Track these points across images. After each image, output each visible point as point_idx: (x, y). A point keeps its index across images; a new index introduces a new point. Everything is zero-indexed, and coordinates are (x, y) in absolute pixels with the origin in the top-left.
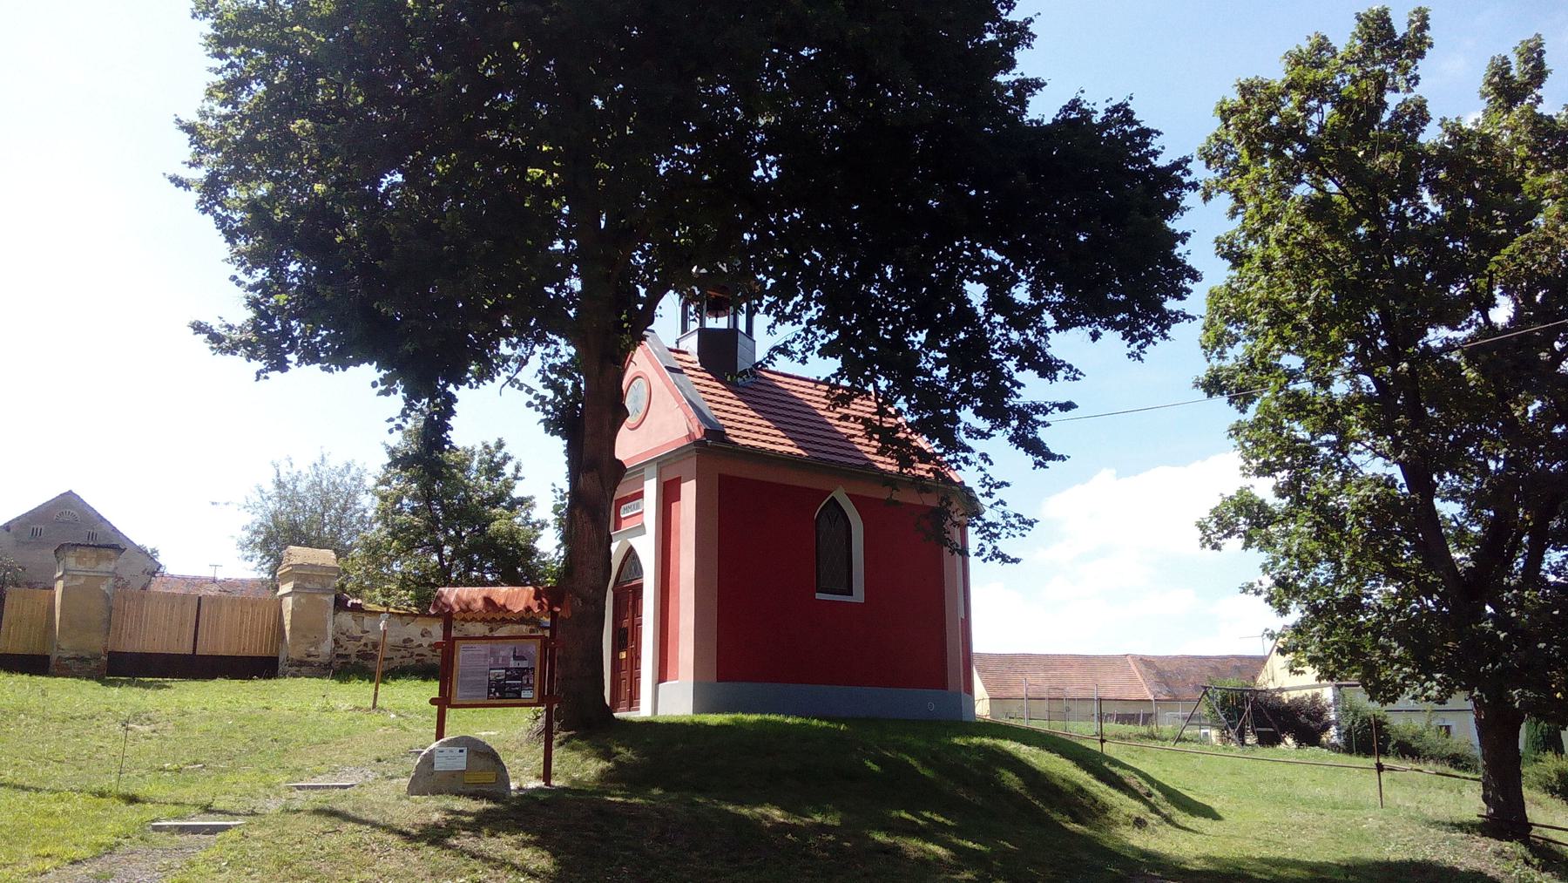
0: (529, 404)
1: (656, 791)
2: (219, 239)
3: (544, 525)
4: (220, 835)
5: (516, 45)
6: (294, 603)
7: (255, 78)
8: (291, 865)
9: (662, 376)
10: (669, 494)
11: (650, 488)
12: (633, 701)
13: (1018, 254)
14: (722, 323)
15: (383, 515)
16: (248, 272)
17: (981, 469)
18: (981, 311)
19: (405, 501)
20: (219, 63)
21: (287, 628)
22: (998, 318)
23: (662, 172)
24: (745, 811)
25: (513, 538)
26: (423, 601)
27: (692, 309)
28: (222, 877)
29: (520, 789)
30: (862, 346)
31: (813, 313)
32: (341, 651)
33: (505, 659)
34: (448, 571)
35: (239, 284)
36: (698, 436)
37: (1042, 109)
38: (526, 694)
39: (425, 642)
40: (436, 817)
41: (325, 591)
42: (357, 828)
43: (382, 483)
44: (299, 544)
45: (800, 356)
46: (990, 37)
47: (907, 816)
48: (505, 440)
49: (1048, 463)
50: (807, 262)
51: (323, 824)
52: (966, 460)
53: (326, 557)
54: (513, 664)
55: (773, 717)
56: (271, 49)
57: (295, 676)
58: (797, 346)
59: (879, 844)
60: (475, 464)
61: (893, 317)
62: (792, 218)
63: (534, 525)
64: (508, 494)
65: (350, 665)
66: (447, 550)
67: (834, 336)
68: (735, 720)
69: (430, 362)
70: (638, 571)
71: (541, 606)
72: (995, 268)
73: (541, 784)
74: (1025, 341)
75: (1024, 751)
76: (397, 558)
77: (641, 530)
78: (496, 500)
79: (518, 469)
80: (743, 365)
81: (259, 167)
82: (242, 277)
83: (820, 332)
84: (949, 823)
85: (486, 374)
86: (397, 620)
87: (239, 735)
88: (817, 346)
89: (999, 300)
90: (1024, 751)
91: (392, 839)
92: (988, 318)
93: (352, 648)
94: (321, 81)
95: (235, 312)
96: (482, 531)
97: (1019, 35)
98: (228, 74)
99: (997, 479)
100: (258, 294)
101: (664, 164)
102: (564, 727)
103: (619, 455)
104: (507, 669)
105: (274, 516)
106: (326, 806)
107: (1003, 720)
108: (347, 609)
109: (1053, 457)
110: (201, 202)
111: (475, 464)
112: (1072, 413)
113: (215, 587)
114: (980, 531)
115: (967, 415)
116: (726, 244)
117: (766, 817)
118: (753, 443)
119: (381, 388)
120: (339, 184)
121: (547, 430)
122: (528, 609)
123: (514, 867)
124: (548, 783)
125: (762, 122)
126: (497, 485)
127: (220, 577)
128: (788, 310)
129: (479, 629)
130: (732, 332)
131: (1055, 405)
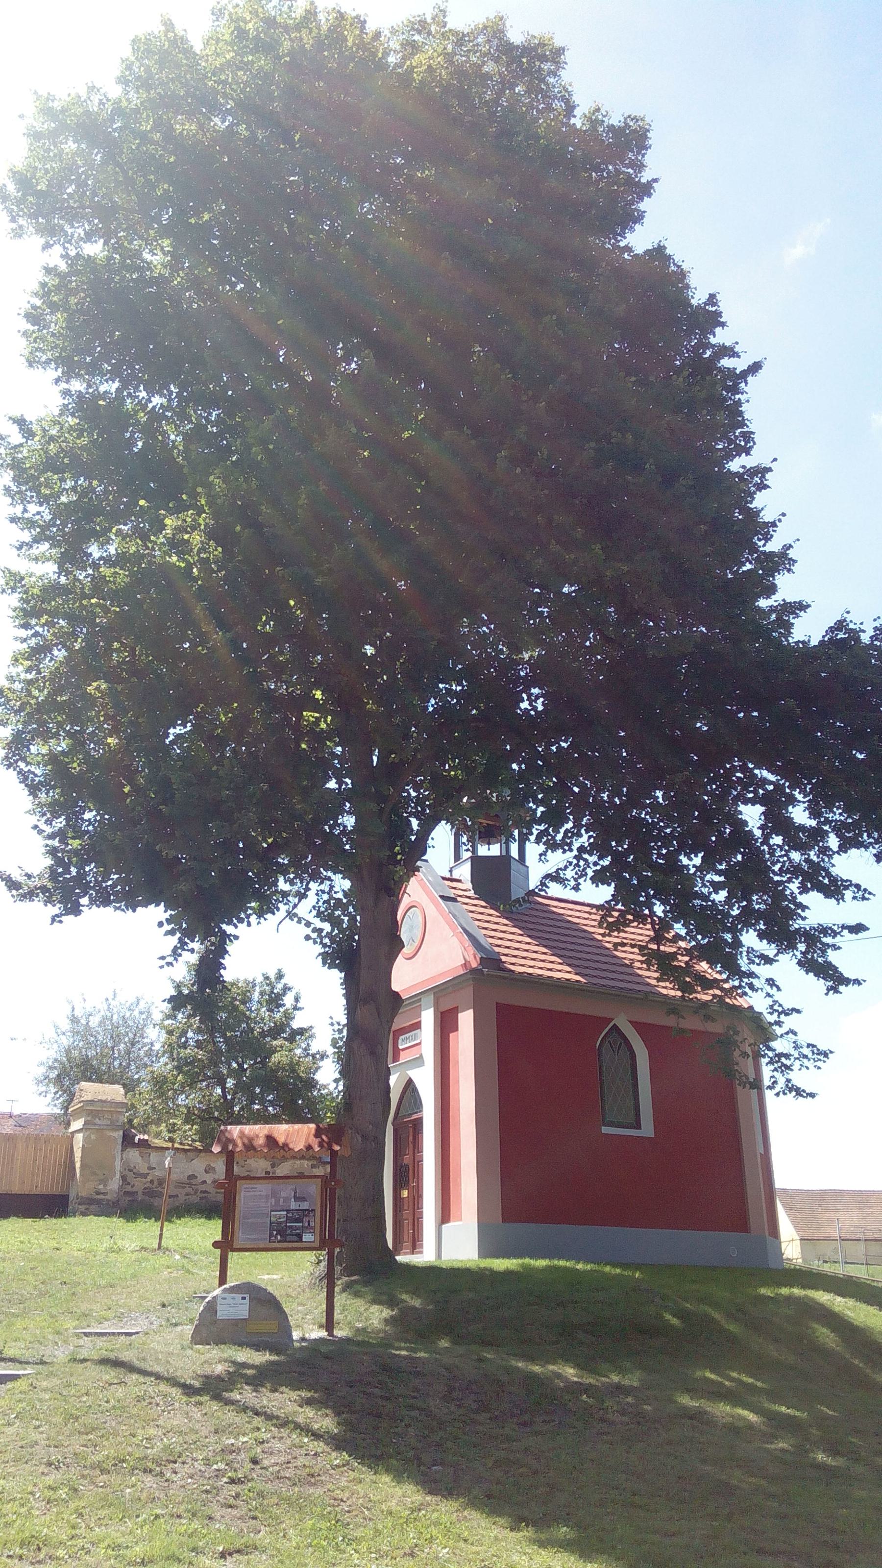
0: (308, 938)
1: (444, 1343)
2: (22, 791)
3: (323, 1056)
4: (10, 1385)
5: (292, 603)
6: (85, 1139)
7: (56, 645)
8: (77, 1418)
9: (437, 906)
10: (446, 1024)
11: (428, 1018)
12: (416, 1244)
13: (793, 773)
14: (494, 850)
15: (169, 1049)
16: (49, 822)
17: (768, 995)
18: (758, 833)
19: (190, 1034)
20: (23, 633)
21: (78, 1165)
22: (777, 840)
23: (431, 709)
24: (537, 1369)
25: (293, 1071)
26: (208, 1137)
27: (464, 839)
28: (10, 1430)
29: (303, 1339)
30: (634, 872)
31: (584, 839)
32: (128, 1188)
33: (287, 1200)
34: (230, 1105)
35: (41, 832)
36: (474, 965)
37: (808, 630)
38: (307, 1237)
39: (209, 1178)
40: (219, 1369)
41: (113, 1126)
42: (142, 1379)
43: (168, 1017)
44: (90, 1080)
45: (573, 883)
46: (748, 566)
47: (713, 1376)
48: (284, 971)
49: (842, 988)
50: (576, 789)
51: (109, 1374)
52: (751, 986)
53: (115, 1092)
54: (293, 1205)
55: (562, 1263)
56: (71, 618)
57: (84, 1214)
58: (569, 873)
59: (685, 1408)
60: (256, 996)
61: (666, 840)
62: (560, 748)
63: (313, 1056)
64: (288, 1025)
65: (138, 1202)
66: (230, 1083)
67: (606, 862)
68: (522, 1265)
69: (207, 908)
70: (417, 1104)
71: (321, 1145)
72: (771, 787)
73: (323, 1334)
74: (808, 861)
75: (839, 1303)
76: (182, 1092)
77: (419, 1061)
78: (277, 1030)
79: (297, 1000)
80: (517, 893)
81: (60, 725)
82: (43, 826)
83: (592, 859)
84: (759, 1384)
85: (266, 908)
86: (181, 1155)
87: (30, 1278)
88: (590, 873)
89: (777, 821)
90: (839, 1303)
91: (175, 1392)
92: (765, 842)
93: (139, 1185)
94: (116, 645)
95: (32, 857)
96: (264, 1063)
97: (780, 561)
98: (33, 642)
99: (787, 1006)
100: (56, 843)
101: (433, 701)
102: (348, 1272)
103: (396, 986)
104: (288, 1211)
105: (68, 1051)
106: (112, 1356)
107: (816, 1265)
108: (134, 1145)
109: (846, 981)
110: (7, 758)
111: (256, 996)
112: (861, 935)
113: (12, 1122)
114: (771, 1062)
115: (750, 938)
116: (492, 776)
117: (559, 1376)
118: (530, 971)
119: (167, 927)
120: (130, 739)
121: (324, 963)
122: (309, 1147)
123: (297, 1426)
124: (331, 1334)
125: (526, 656)
126: (278, 1016)
127: (16, 1112)
128: (559, 837)
129: (260, 1166)
130: (505, 859)
131: (844, 927)
